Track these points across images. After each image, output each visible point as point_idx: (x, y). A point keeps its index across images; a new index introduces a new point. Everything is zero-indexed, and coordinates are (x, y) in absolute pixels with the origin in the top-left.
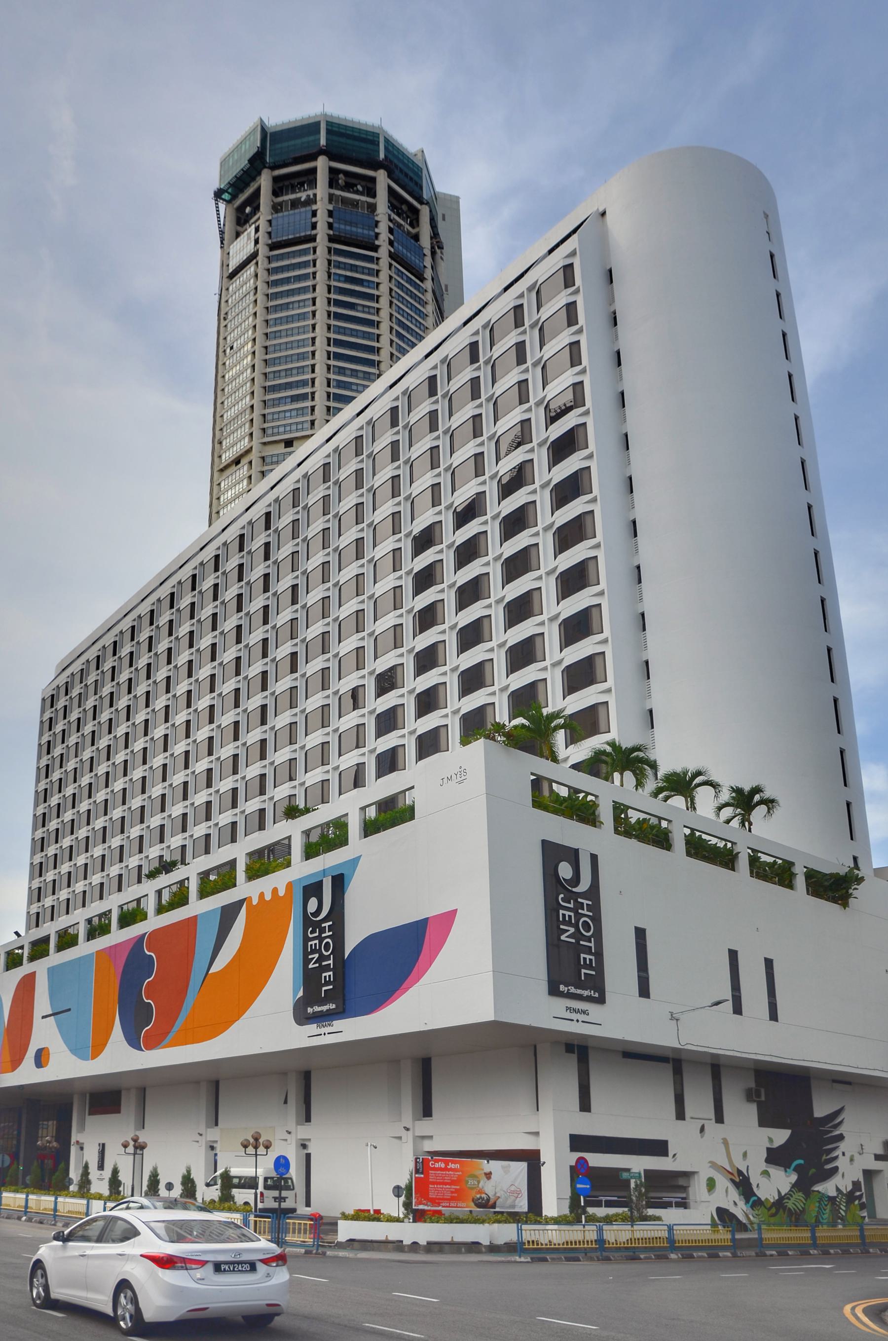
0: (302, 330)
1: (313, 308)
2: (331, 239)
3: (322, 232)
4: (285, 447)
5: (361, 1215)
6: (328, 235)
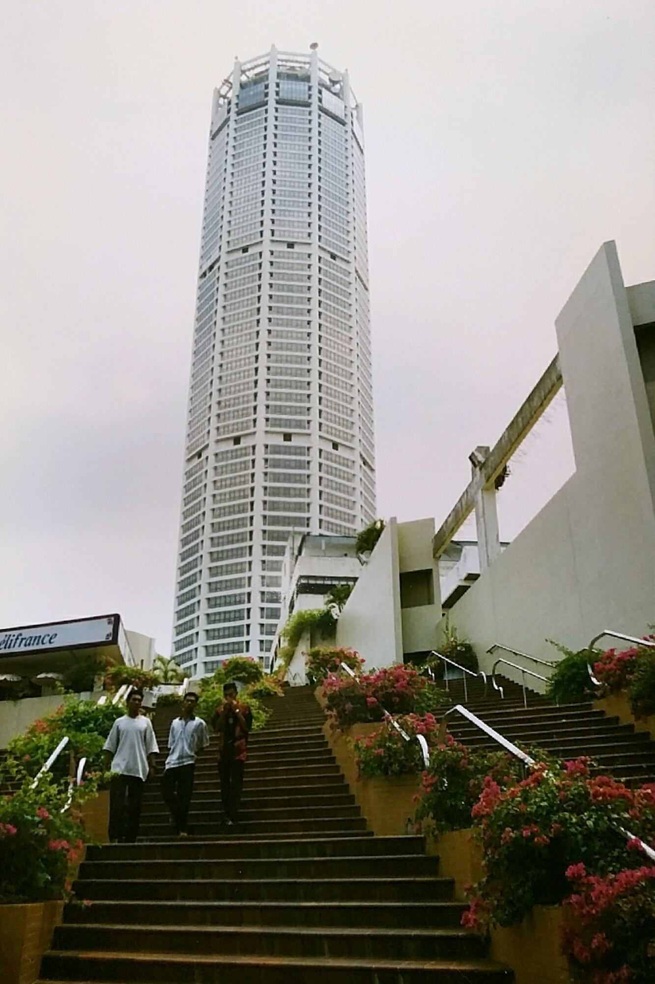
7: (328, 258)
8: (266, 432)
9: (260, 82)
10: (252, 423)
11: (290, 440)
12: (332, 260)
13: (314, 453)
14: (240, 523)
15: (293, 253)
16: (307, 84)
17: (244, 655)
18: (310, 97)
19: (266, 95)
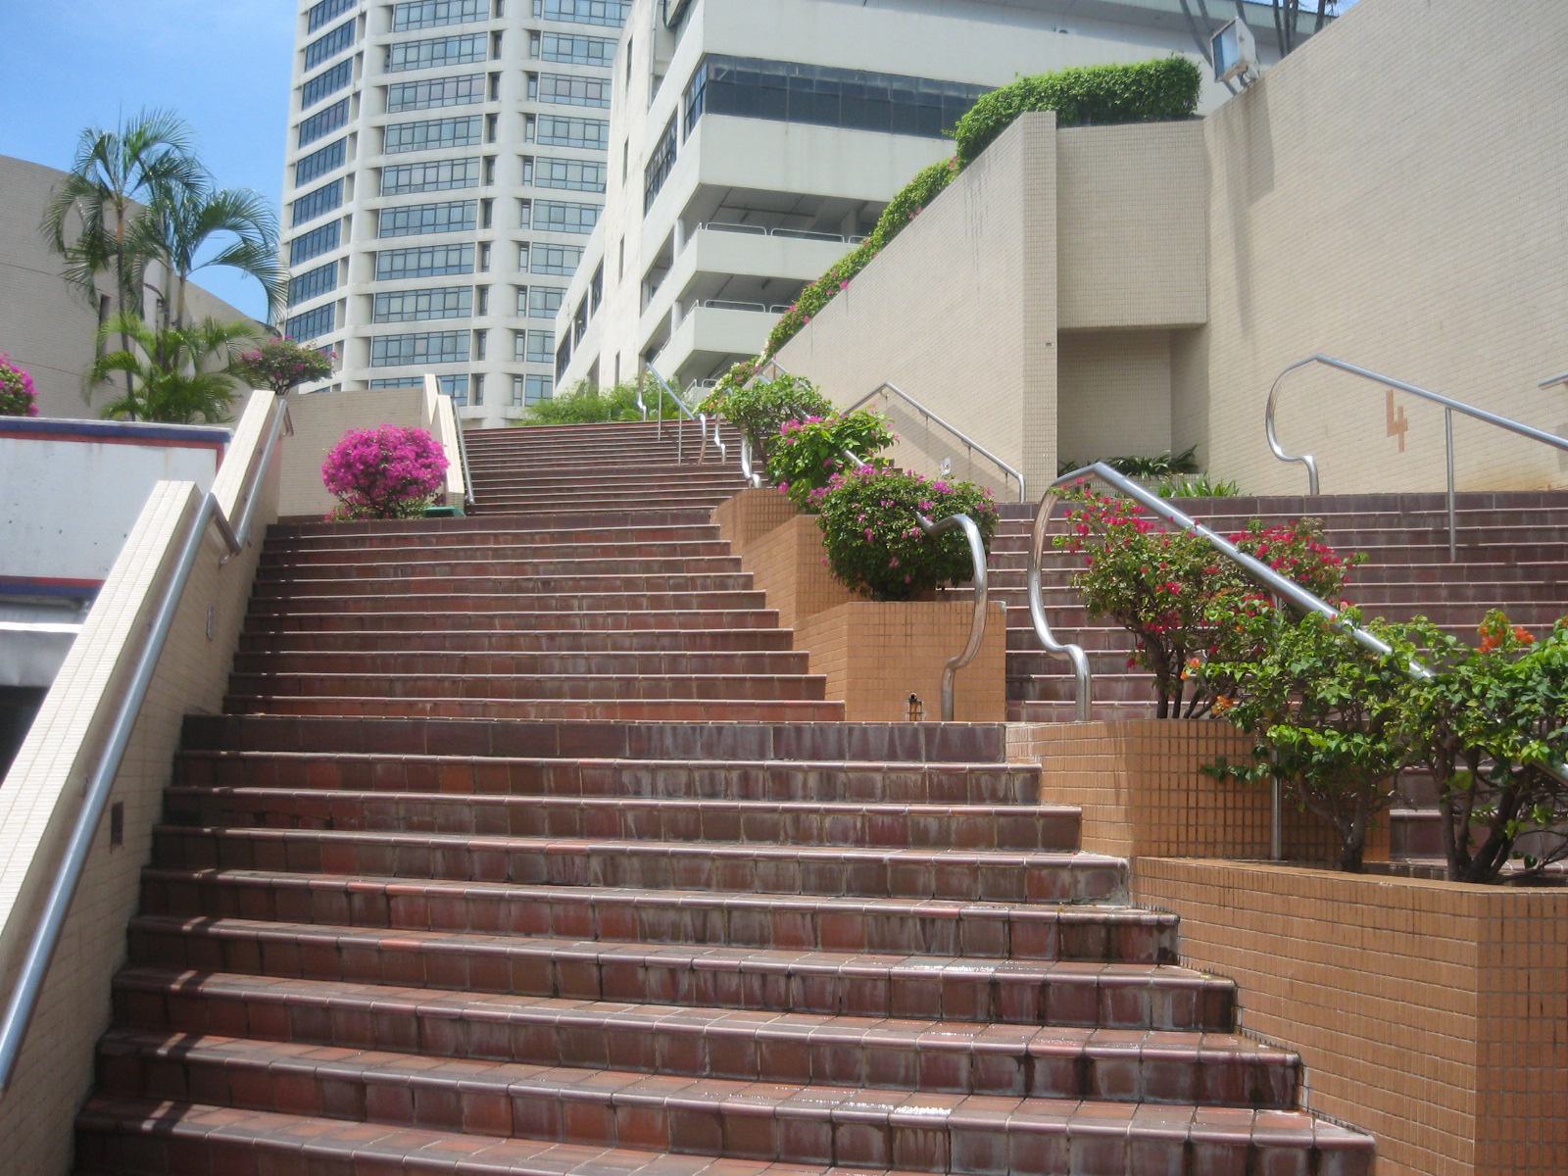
5: (649, 354)
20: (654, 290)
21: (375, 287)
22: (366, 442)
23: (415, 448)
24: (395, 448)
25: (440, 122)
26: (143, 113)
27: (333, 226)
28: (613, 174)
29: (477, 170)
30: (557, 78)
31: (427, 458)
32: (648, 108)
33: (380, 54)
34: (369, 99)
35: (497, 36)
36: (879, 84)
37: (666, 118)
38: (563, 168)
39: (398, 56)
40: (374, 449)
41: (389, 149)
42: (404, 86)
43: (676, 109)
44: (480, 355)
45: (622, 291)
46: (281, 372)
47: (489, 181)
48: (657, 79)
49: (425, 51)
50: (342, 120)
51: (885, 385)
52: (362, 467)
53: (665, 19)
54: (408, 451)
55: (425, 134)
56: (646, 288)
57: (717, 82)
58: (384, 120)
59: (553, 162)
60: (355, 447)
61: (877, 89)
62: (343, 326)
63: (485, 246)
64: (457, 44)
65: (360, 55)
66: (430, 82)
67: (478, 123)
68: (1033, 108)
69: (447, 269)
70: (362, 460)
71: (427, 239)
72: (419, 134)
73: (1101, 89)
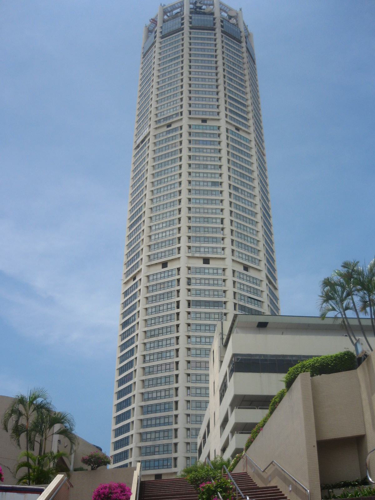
0: (174, 145)
1: (177, 311)
2: (191, 28)
3: (186, 26)
4: (163, 268)
5: (224, 450)
6: (190, 27)
7: (234, 129)
8: (189, 257)
9: (178, 17)
10: (177, 251)
11: (209, 264)
12: (245, 272)
13: (229, 273)
14: (165, 463)
15: (209, 269)
16: (212, 16)
17: (173, 470)
18: (214, 24)
19: (182, 24)
20: (224, 428)
21: (142, 431)
22: (105, 488)
23: (120, 489)
24: (114, 490)
25: (161, 378)
26: (34, 389)
27: (129, 412)
28: (211, 391)
29: (173, 392)
30: (196, 362)
31: (124, 492)
32: (219, 371)
33: (142, 358)
34: (139, 372)
35: (177, 350)
36: (289, 358)
37: (224, 374)
38: (200, 390)
39: (147, 358)
40: (107, 490)
41: (146, 387)
42: (149, 367)
43: (227, 371)
44: (176, 451)
45: (215, 430)
46: (95, 463)
47: (177, 395)
48: (221, 362)
49: (156, 356)
50: (131, 379)
51: (273, 462)
52: (103, 496)
53: (223, 344)
54: (119, 490)
55: (156, 382)
56: (222, 428)
57: (238, 362)
58: (144, 378)
59: (196, 388)
60: (102, 489)
61: (288, 360)
62: (132, 443)
63: (176, 416)
64: (165, 353)
65: (136, 358)
66: (158, 366)
67: (172, 377)
68: (304, 372)
69: (164, 424)
70: (103, 493)
71: (158, 415)
72: (155, 382)
73: (325, 363)
